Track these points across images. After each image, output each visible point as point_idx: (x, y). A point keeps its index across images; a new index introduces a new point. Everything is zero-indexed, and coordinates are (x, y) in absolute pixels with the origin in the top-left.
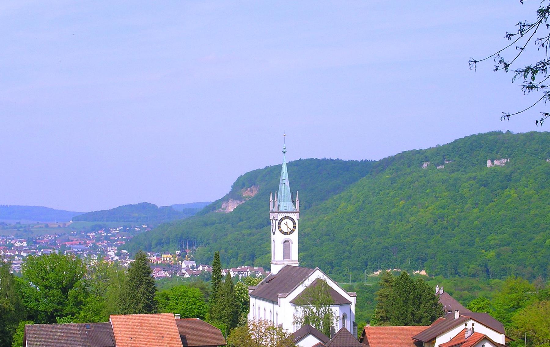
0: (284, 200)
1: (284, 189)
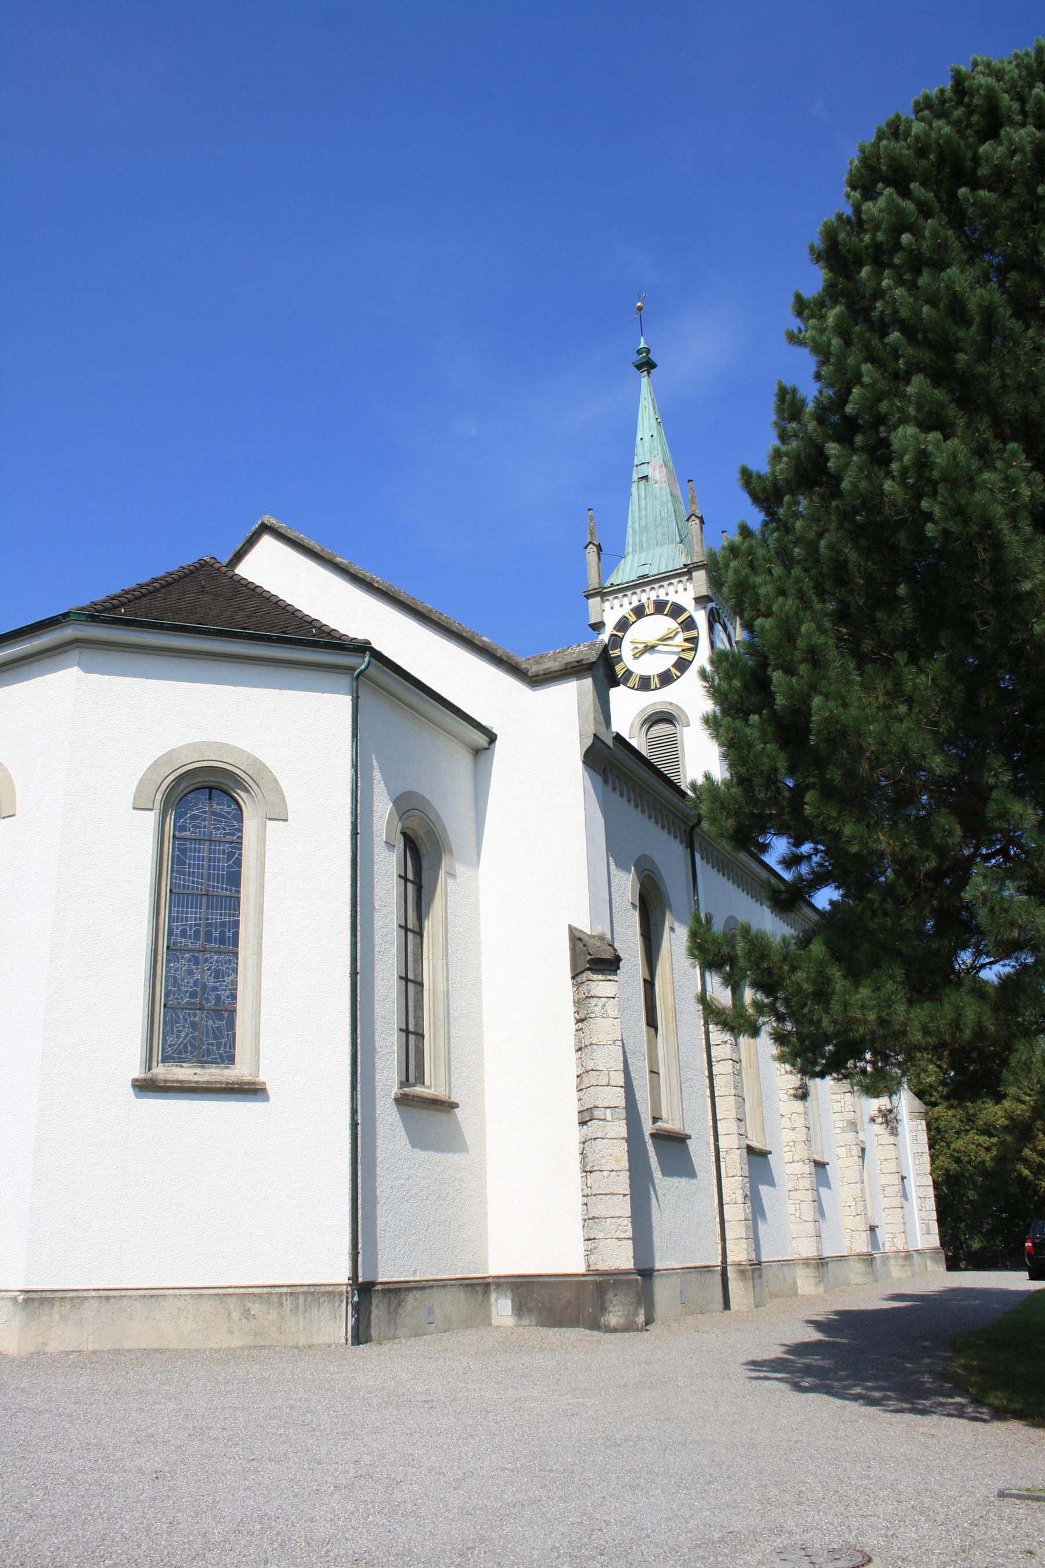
0: (644, 545)
1: (643, 503)
